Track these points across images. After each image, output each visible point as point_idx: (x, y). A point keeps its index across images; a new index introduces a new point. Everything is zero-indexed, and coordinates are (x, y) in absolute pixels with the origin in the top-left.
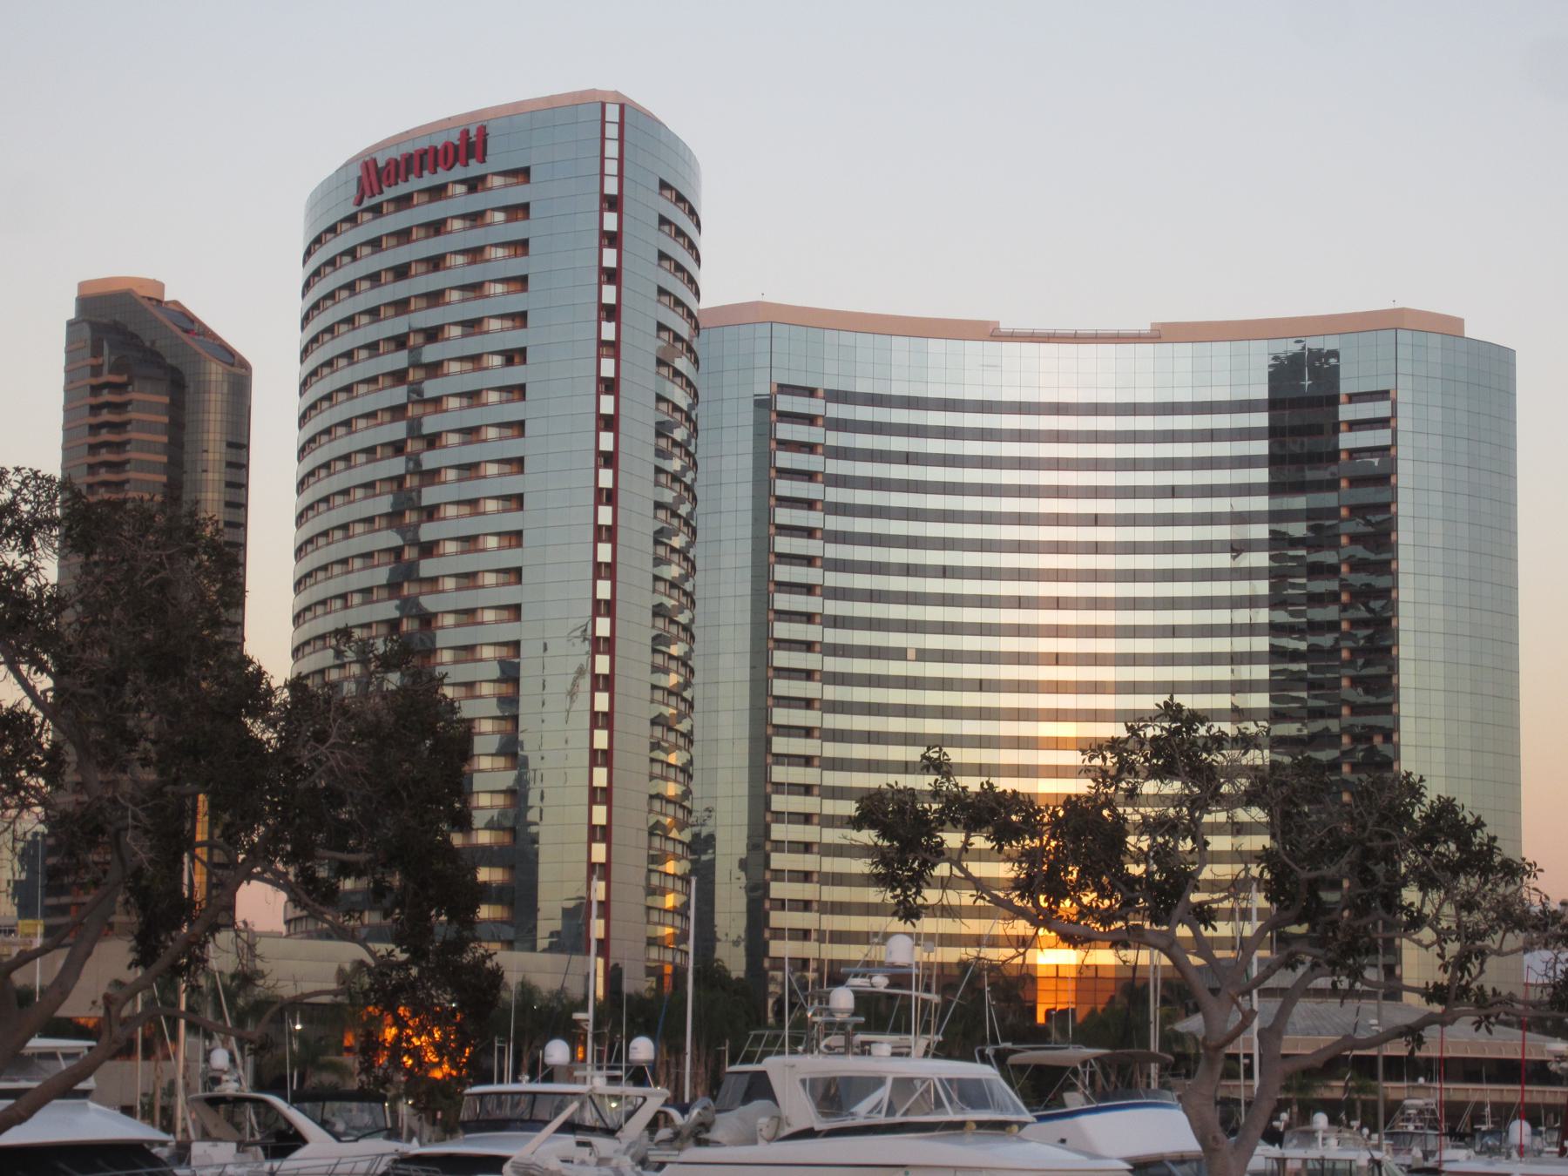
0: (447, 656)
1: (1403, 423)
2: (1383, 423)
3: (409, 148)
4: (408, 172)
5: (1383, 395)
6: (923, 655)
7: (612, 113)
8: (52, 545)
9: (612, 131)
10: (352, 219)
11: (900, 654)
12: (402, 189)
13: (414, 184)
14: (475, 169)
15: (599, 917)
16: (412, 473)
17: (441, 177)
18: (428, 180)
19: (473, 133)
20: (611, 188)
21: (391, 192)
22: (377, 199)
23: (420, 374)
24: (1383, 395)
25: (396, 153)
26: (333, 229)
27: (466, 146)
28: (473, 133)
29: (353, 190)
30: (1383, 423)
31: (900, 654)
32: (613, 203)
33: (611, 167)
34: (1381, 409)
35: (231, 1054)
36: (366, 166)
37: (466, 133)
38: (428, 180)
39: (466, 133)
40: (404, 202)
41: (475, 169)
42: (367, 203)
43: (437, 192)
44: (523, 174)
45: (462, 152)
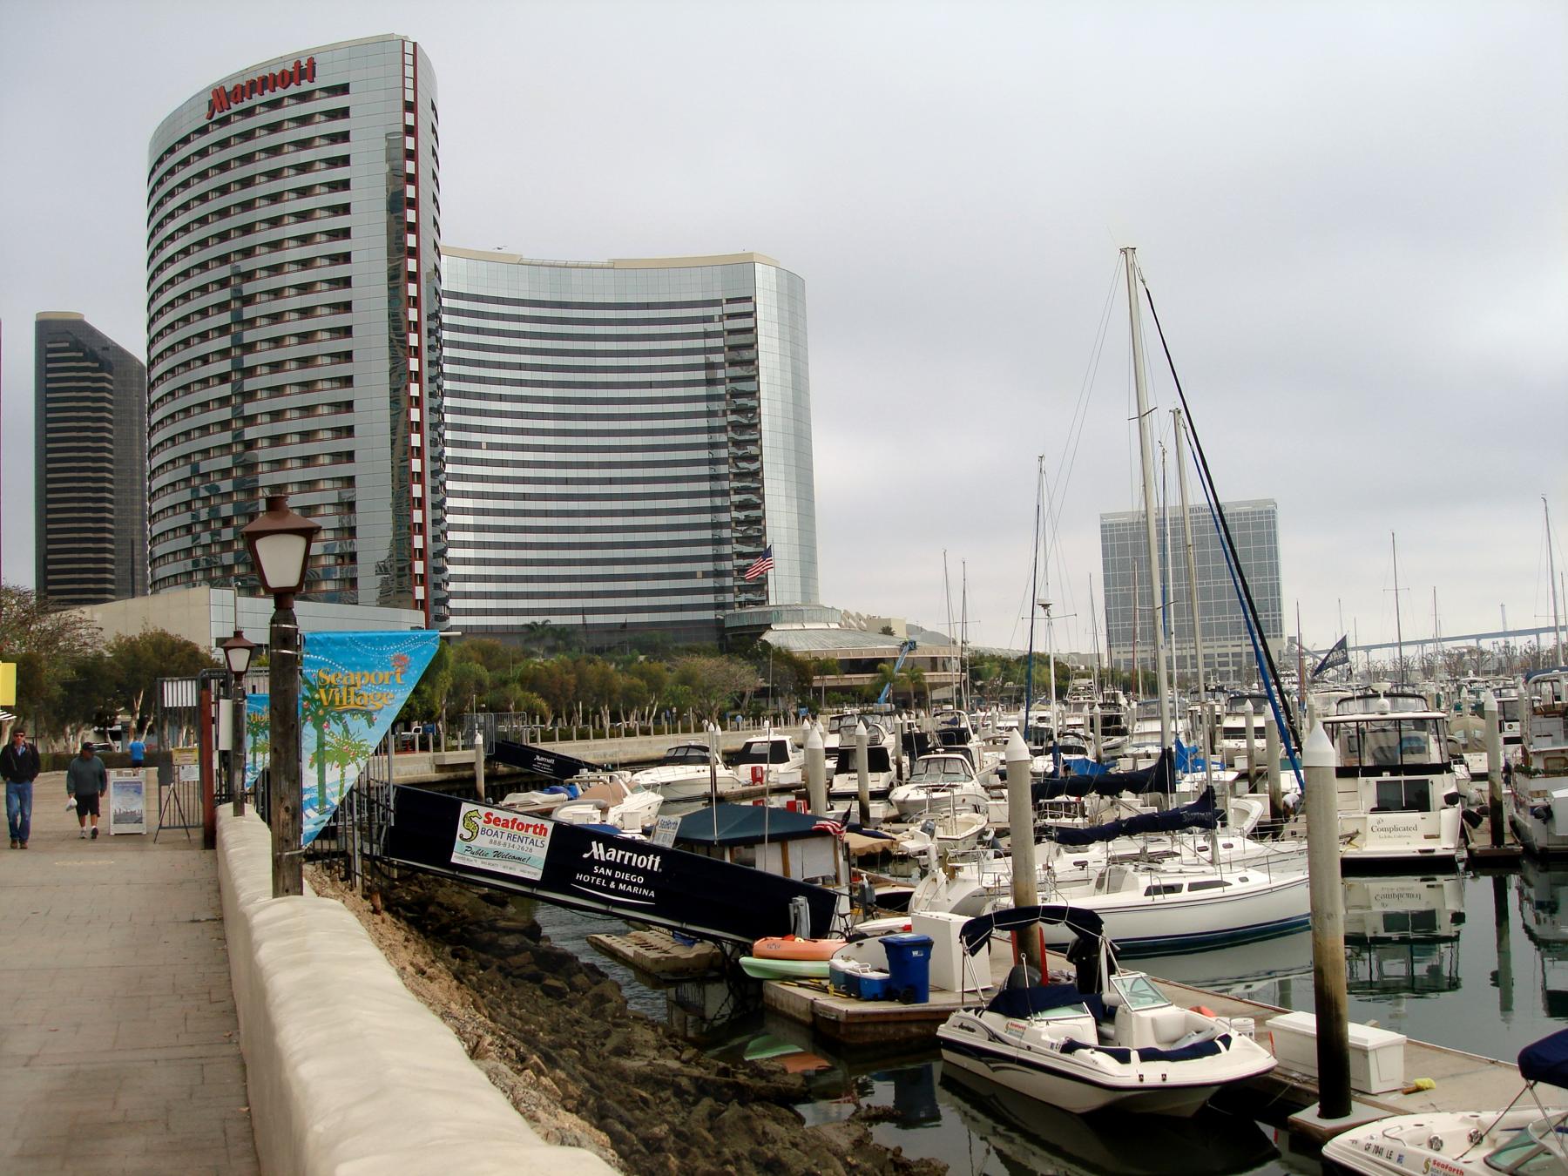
1: (760, 315)
3: (261, 74)
4: (264, 88)
5: (748, 299)
6: (491, 446)
7: (409, 49)
9: (409, 59)
10: (203, 131)
11: (477, 445)
12: (247, 104)
13: (257, 99)
14: (306, 86)
15: (925, 1000)
16: (235, 299)
17: (280, 92)
18: (268, 96)
19: (304, 63)
20: (410, 97)
21: (235, 108)
22: (226, 113)
23: (238, 280)
24: (748, 299)
26: (171, 150)
27: (304, 70)
28: (304, 63)
29: (205, 109)
30: (749, 315)
31: (477, 445)
32: (410, 107)
33: (409, 83)
34: (747, 307)
37: (298, 64)
38: (268, 96)
39: (298, 64)
40: (249, 113)
41: (306, 86)
42: (217, 116)
43: (275, 104)
44: (344, 89)
45: (296, 76)
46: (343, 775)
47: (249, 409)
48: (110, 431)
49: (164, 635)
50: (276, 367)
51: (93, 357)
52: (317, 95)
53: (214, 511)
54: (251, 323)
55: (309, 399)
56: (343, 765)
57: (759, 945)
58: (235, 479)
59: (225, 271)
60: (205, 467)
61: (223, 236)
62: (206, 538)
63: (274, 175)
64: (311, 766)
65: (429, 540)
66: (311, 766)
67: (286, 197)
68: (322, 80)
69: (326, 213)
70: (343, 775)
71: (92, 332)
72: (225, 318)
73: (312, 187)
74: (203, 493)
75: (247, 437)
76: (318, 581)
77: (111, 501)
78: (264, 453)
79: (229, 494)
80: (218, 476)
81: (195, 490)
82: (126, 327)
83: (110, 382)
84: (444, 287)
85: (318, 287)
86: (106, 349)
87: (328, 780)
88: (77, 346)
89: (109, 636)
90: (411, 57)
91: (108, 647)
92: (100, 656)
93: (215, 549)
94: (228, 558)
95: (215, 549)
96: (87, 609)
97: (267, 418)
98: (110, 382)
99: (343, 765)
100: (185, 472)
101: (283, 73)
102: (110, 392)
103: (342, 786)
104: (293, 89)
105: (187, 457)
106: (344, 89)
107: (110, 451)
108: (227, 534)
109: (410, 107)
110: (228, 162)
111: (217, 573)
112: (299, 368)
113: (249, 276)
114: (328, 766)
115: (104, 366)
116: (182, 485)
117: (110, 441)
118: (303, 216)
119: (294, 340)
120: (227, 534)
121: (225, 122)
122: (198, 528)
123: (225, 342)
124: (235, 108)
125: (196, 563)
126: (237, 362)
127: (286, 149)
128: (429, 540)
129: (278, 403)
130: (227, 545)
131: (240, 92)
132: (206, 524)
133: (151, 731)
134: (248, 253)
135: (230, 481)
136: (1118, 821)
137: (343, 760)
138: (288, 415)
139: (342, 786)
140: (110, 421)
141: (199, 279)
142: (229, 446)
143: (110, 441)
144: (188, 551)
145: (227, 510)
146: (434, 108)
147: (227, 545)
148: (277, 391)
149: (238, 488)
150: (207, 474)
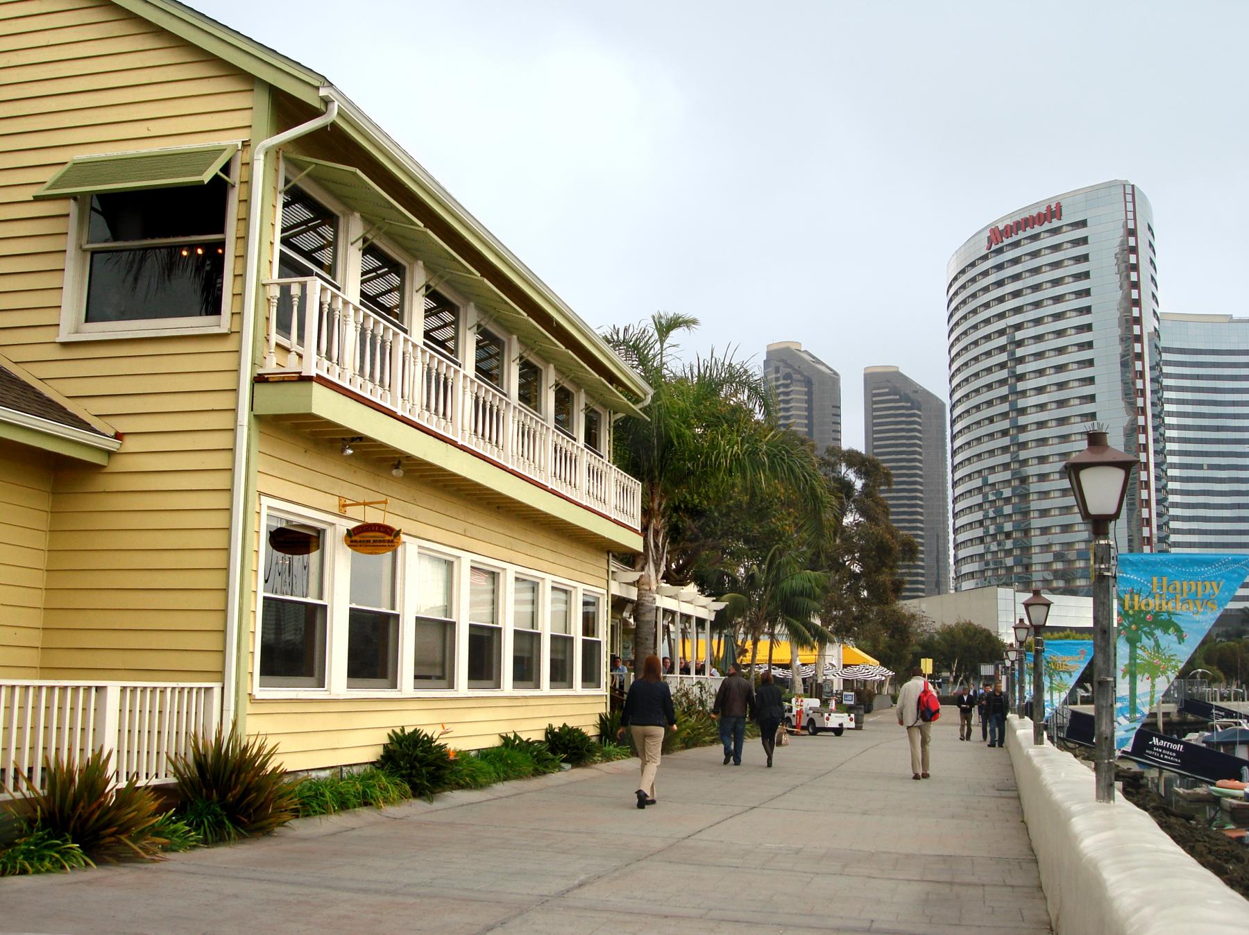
0: (1037, 550)
2: (876, 402)
6: (1200, 467)
7: (1129, 190)
8: (828, 557)
9: (1129, 198)
12: (1015, 238)
13: (1021, 235)
14: (1056, 223)
16: (1010, 343)
17: (1037, 229)
18: (1030, 232)
19: (1053, 206)
20: (1131, 225)
21: (1007, 241)
22: (1000, 245)
23: (1012, 347)
25: (1009, 222)
27: (1054, 212)
28: (1053, 206)
29: (985, 243)
30: (876, 402)
31: (1211, 467)
33: (1130, 215)
35: (134, 259)
36: (992, 231)
37: (1049, 207)
38: (1030, 232)
39: (1049, 207)
40: (1016, 244)
41: (1056, 223)
42: (994, 247)
43: (1035, 238)
44: (1083, 224)
46: (1153, 686)
47: (1022, 438)
48: (920, 454)
49: (970, 624)
50: (1041, 425)
51: (906, 398)
52: (1064, 229)
53: (1000, 529)
54: (1023, 393)
55: (1064, 430)
56: (1153, 677)
57: (1219, 782)
58: (1015, 557)
59: (1003, 341)
60: (992, 479)
61: (1001, 316)
62: (994, 547)
63: (1036, 288)
64: (1123, 677)
65: (1155, 530)
66: (1123, 677)
67: (1045, 303)
68: (1067, 219)
69: (1074, 314)
70: (1153, 686)
71: (905, 379)
72: (1004, 390)
73: (1062, 279)
74: (991, 498)
75: (1021, 458)
76: (1074, 579)
77: (921, 506)
78: (1035, 487)
79: (1010, 515)
80: (1001, 486)
81: (985, 496)
82: (932, 373)
83: (919, 417)
84: (1162, 344)
85: (1070, 367)
86: (916, 392)
87: (1138, 692)
88: (894, 391)
89: (938, 626)
90: (1130, 193)
91: (938, 633)
92: (932, 637)
93: (1001, 555)
94: (1009, 561)
95: (1001, 555)
96: (915, 601)
97: (1034, 427)
98: (919, 417)
99: (1153, 677)
100: (978, 482)
101: (1039, 214)
102: (919, 424)
103: (1152, 697)
104: (1047, 226)
105: (979, 472)
106: (1083, 224)
107: (920, 469)
108: (1009, 544)
109: (1132, 233)
110: (1004, 313)
111: (1002, 572)
112: (1058, 408)
113: (1020, 344)
114: (1139, 677)
115: (915, 405)
116: (976, 475)
117: (920, 461)
118: (1058, 316)
119: (1054, 406)
120: (1009, 544)
121: (1000, 251)
122: (988, 539)
123: (1005, 407)
124: (1007, 241)
125: (987, 564)
126: (1013, 438)
127: (1044, 269)
128: (1155, 530)
129: (1043, 433)
130: (1008, 553)
131: (1010, 230)
132: (994, 536)
133: (962, 683)
134: (1018, 327)
135: (1007, 387)
136: (510, 744)
137: (1154, 671)
138: (1051, 459)
139: (1152, 697)
140: (920, 446)
141: (986, 396)
142: (1009, 481)
143: (920, 461)
144: (981, 556)
145: (1008, 527)
146: (1150, 228)
147: (1008, 553)
148: (1043, 441)
149: (1018, 562)
150: (994, 484)
